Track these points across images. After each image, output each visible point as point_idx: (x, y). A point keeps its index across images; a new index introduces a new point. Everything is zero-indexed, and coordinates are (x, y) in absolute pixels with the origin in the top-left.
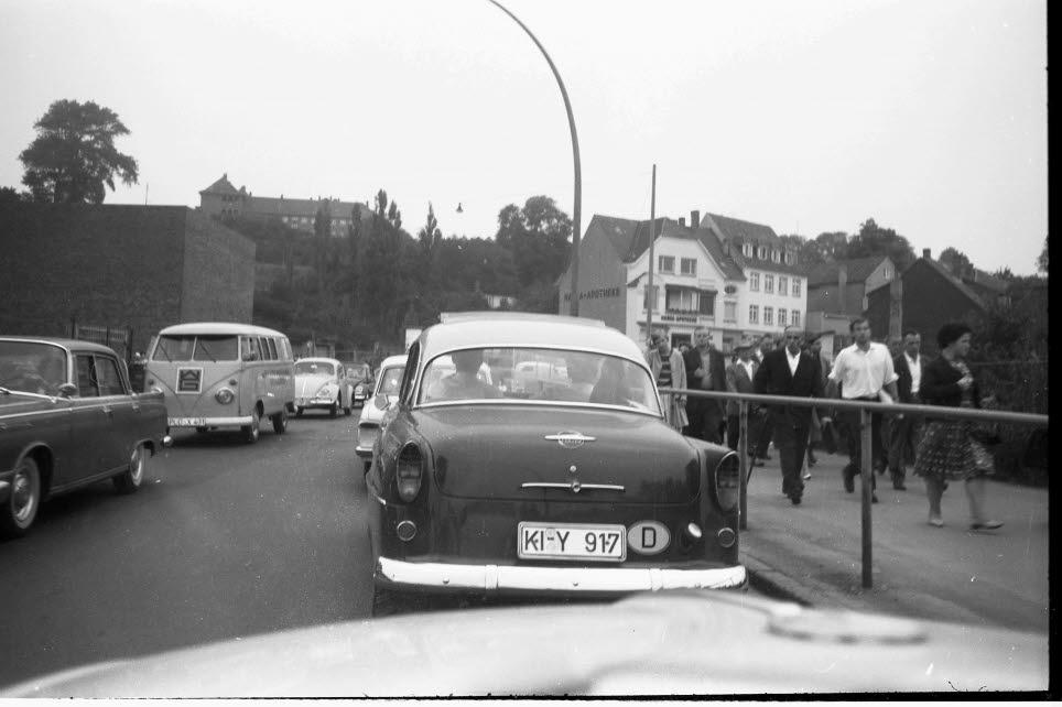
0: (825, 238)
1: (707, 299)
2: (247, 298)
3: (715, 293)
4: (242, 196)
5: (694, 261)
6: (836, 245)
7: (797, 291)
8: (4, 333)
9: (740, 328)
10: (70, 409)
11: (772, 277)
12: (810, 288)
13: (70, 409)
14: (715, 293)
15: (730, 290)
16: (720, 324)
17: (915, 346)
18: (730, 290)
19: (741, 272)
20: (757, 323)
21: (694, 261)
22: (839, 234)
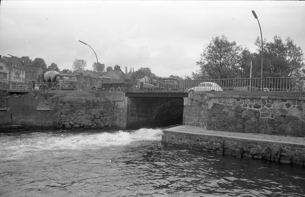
0: (23, 57)
1: (6, 74)
2: (124, 125)
3: (7, 74)
4: (150, 71)
5: (2, 67)
6: (26, 60)
7: (23, 73)
8: (1, 107)
9: (12, 81)
10: (56, 149)
11: (15, 70)
12: (26, 73)
13: (56, 149)
14: (7, 74)
15: (10, 73)
16: (8, 80)
17: (53, 83)
18: (10, 73)
19: (12, 69)
20: (15, 80)
21: (2, 67)
22: (27, 57)
